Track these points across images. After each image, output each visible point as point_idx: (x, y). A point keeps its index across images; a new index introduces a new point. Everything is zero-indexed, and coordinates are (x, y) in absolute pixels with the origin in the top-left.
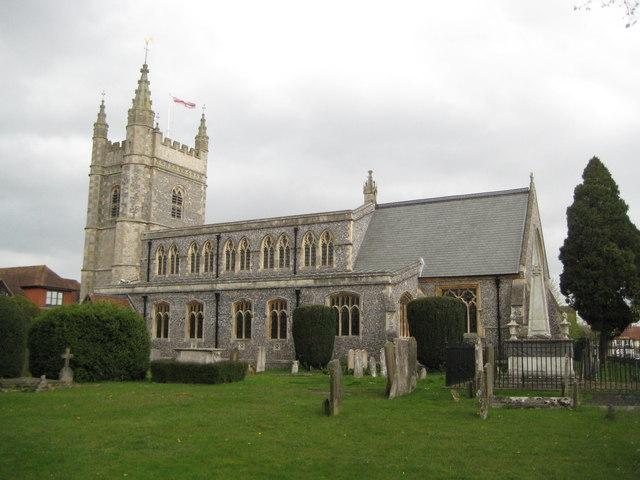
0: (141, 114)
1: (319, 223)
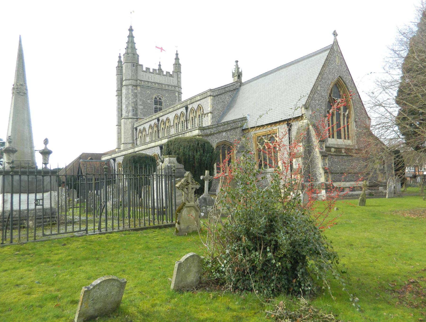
0: (131, 55)
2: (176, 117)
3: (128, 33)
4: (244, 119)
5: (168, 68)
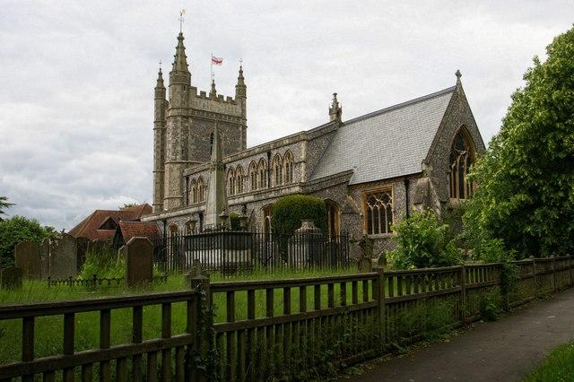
0: (181, 74)
3: (176, 42)
4: (350, 173)
5: (228, 90)
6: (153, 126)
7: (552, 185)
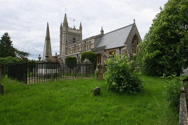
0: (66, 23)
1: (89, 40)
2: (81, 45)
4: (105, 46)
5: (78, 28)
6: (59, 36)
7: (169, 48)
